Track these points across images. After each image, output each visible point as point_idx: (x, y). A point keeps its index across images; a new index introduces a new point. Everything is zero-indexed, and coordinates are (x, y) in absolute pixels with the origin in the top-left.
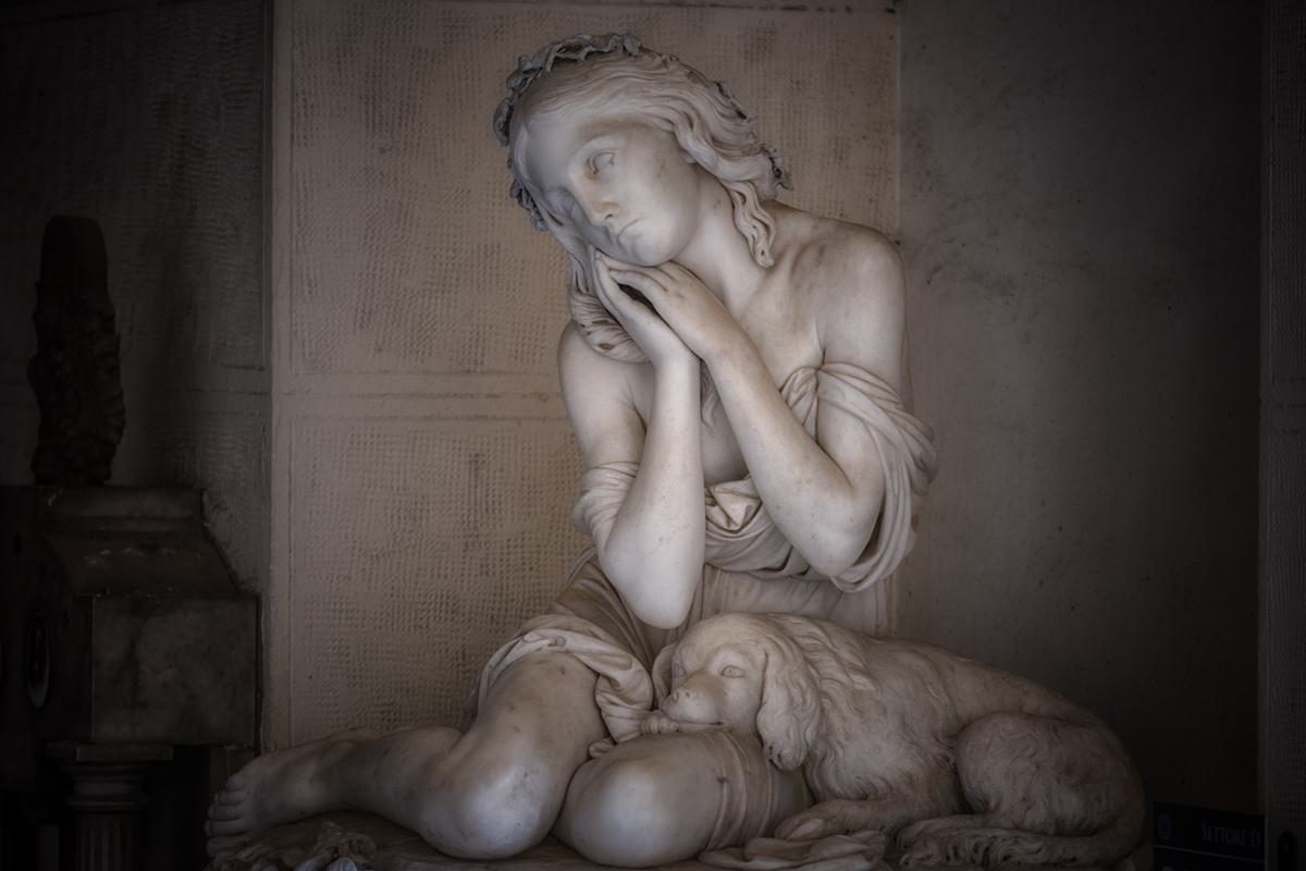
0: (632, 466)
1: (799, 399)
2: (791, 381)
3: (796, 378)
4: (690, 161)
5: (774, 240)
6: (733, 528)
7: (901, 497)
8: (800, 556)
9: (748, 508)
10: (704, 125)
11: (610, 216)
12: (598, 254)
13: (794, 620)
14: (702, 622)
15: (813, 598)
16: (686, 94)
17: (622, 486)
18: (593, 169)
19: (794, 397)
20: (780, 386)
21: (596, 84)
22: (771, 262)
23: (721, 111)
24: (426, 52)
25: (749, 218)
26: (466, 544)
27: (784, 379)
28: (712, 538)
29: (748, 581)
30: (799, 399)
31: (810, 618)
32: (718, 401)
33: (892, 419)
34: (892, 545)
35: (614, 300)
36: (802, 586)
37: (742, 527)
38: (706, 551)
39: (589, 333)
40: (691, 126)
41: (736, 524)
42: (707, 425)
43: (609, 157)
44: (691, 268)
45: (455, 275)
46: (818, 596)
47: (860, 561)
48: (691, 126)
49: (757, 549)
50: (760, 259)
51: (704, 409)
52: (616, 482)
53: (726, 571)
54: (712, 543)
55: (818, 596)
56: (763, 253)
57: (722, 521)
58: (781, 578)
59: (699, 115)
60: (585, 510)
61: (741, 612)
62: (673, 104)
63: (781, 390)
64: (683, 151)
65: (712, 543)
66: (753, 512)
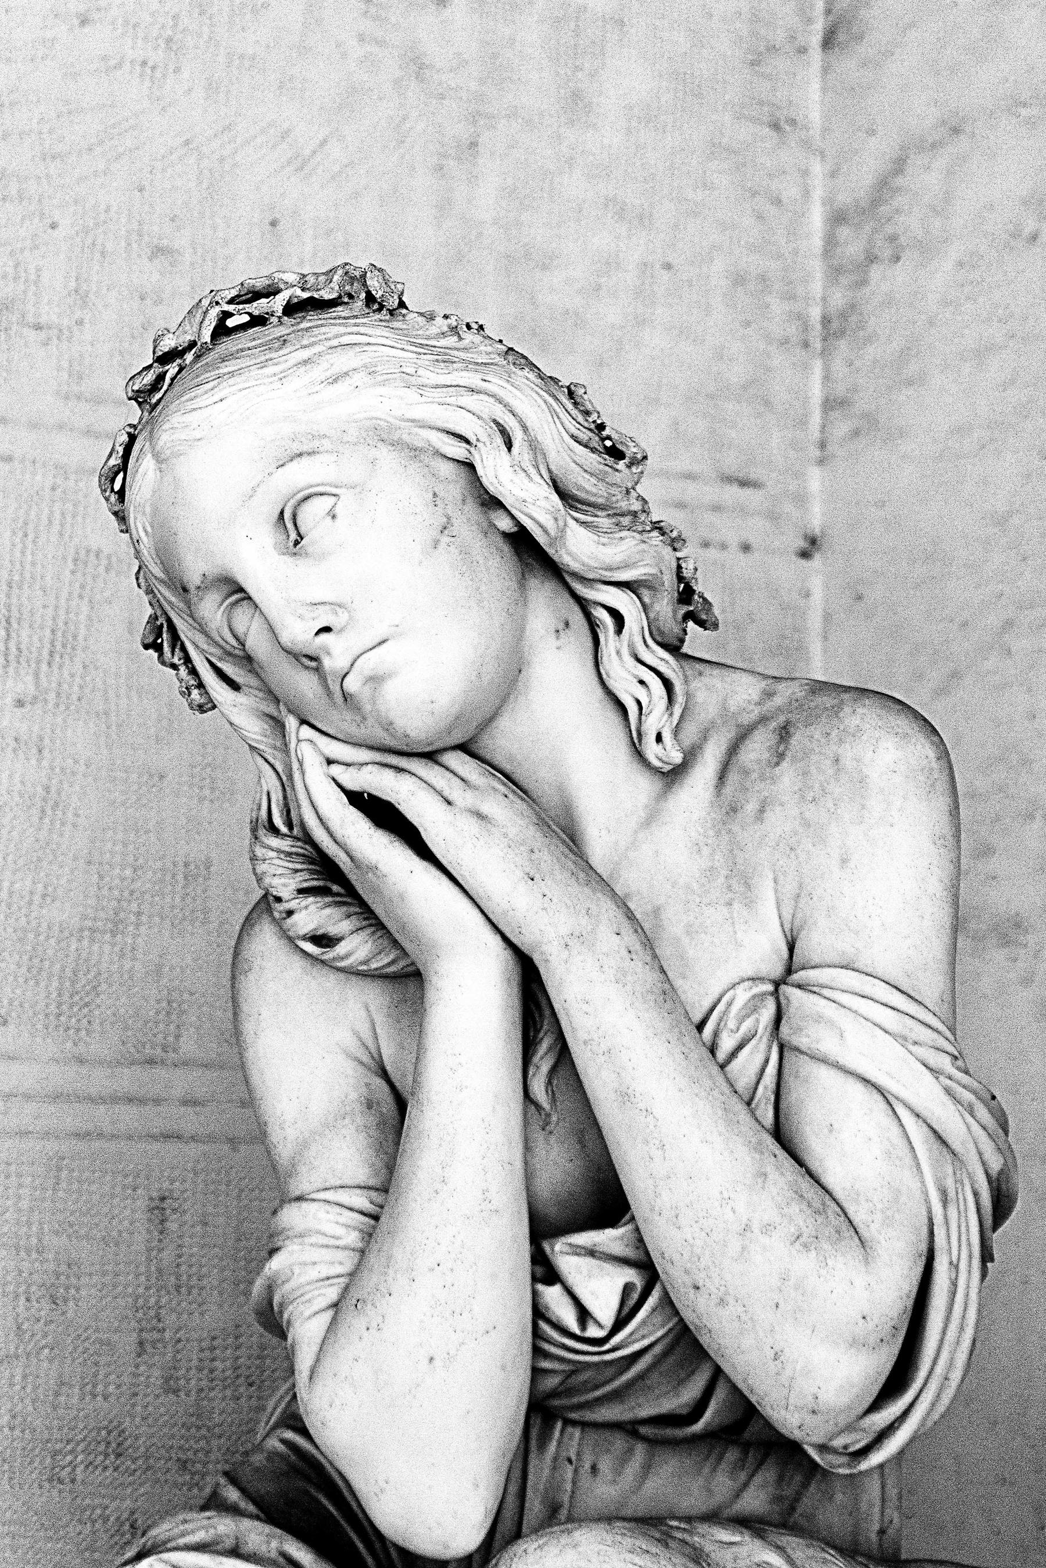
0: (374, 1194)
1: (740, 1047)
2: (720, 1008)
3: (730, 1004)
4: (505, 524)
5: (682, 717)
6: (593, 1332)
7: (963, 1266)
8: (735, 1389)
9: (628, 1288)
10: (534, 446)
11: (327, 629)
12: (306, 732)
13: (725, 1535)
14: (520, 1546)
15: (758, 1479)
16: (496, 384)
17: (353, 1238)
18: (293, 536)
19: (727, 1044)
20: (697, 1017)
21: (305, 354)
22: (677, 757)
23: (576, 433)
24: (97, 556)
25: (631, 662)
26: (141, 1343)
27: (707, 1004)
28: (547, 1355)
29: (619, 1442)
30: (740, 1047)
31: (745, 1523)
32: (563, 1053)
33: (948, 1091)
34: (939, 1370)
35: (335, 825)
36: (732, 1455)
37: (619, 1324)
38: (533, 1381)
39: (290, 913)
40: (509, 445)
41: (600, 1326)
42: (538, 1107)
43: (326, 502)
44: (507, 767)
45: (134, 906)
46: (767, 1475)
47: (876, 1406)
48: (509, 445)
49: (641, 1376)
50: (652, 750)
51: (531, 1071)
52: (340, 1231)
53: (574, 1423)
54: (546, 1364)
55: (767, 1475)
56: (659, 738)
57: (569, 1318)
58: (696, 1438)
59: (525, 428)
60: (270, 1289)
61: (608, 1518)
62: (468, 401)
63: (700, 1027)
64: (491, 503)
65: (546, 1364)
66: (635, 1296)
